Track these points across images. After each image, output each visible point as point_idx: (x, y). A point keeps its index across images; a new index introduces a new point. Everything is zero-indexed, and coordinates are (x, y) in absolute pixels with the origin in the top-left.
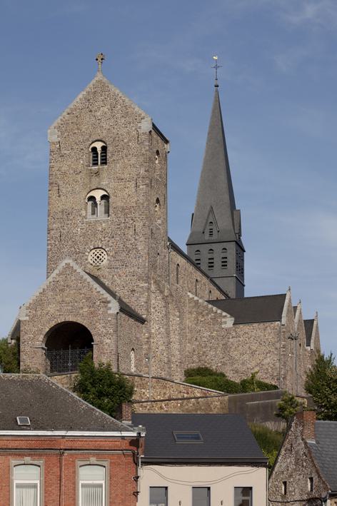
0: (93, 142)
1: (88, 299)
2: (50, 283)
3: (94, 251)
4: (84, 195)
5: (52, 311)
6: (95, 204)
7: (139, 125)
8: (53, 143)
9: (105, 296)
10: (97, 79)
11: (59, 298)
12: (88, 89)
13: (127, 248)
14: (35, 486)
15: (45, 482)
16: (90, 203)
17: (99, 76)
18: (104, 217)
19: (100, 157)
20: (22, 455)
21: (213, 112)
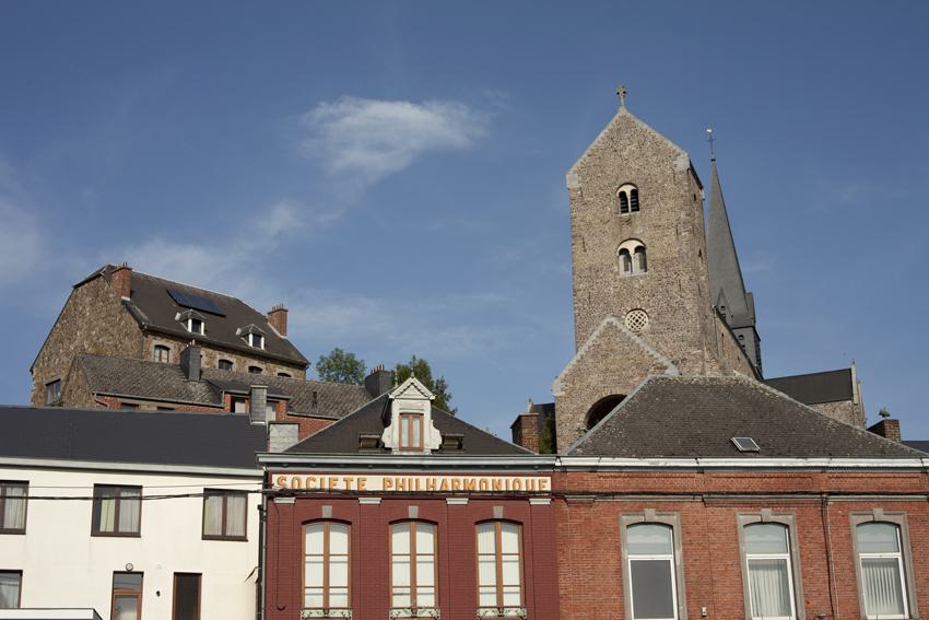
0: (621, 186)
1: (638, 366)
2: (589, 347)
3: (631, 313)
4: (615, 248)
5: (594, 383)
6: (628, 258)
7: (674, 162)
8: (574, 190)
9: (660, 361)
10: (619, 114)
11: (601, 366)
12: (610, 127)
13: (672, 307)
14: (781, 565)
15: (801, 556)
16: (622, 257)
17: (622, 111)
18: (642, 273)
19: (630, 203)
20: (756, 506)
21: (713, 187)
